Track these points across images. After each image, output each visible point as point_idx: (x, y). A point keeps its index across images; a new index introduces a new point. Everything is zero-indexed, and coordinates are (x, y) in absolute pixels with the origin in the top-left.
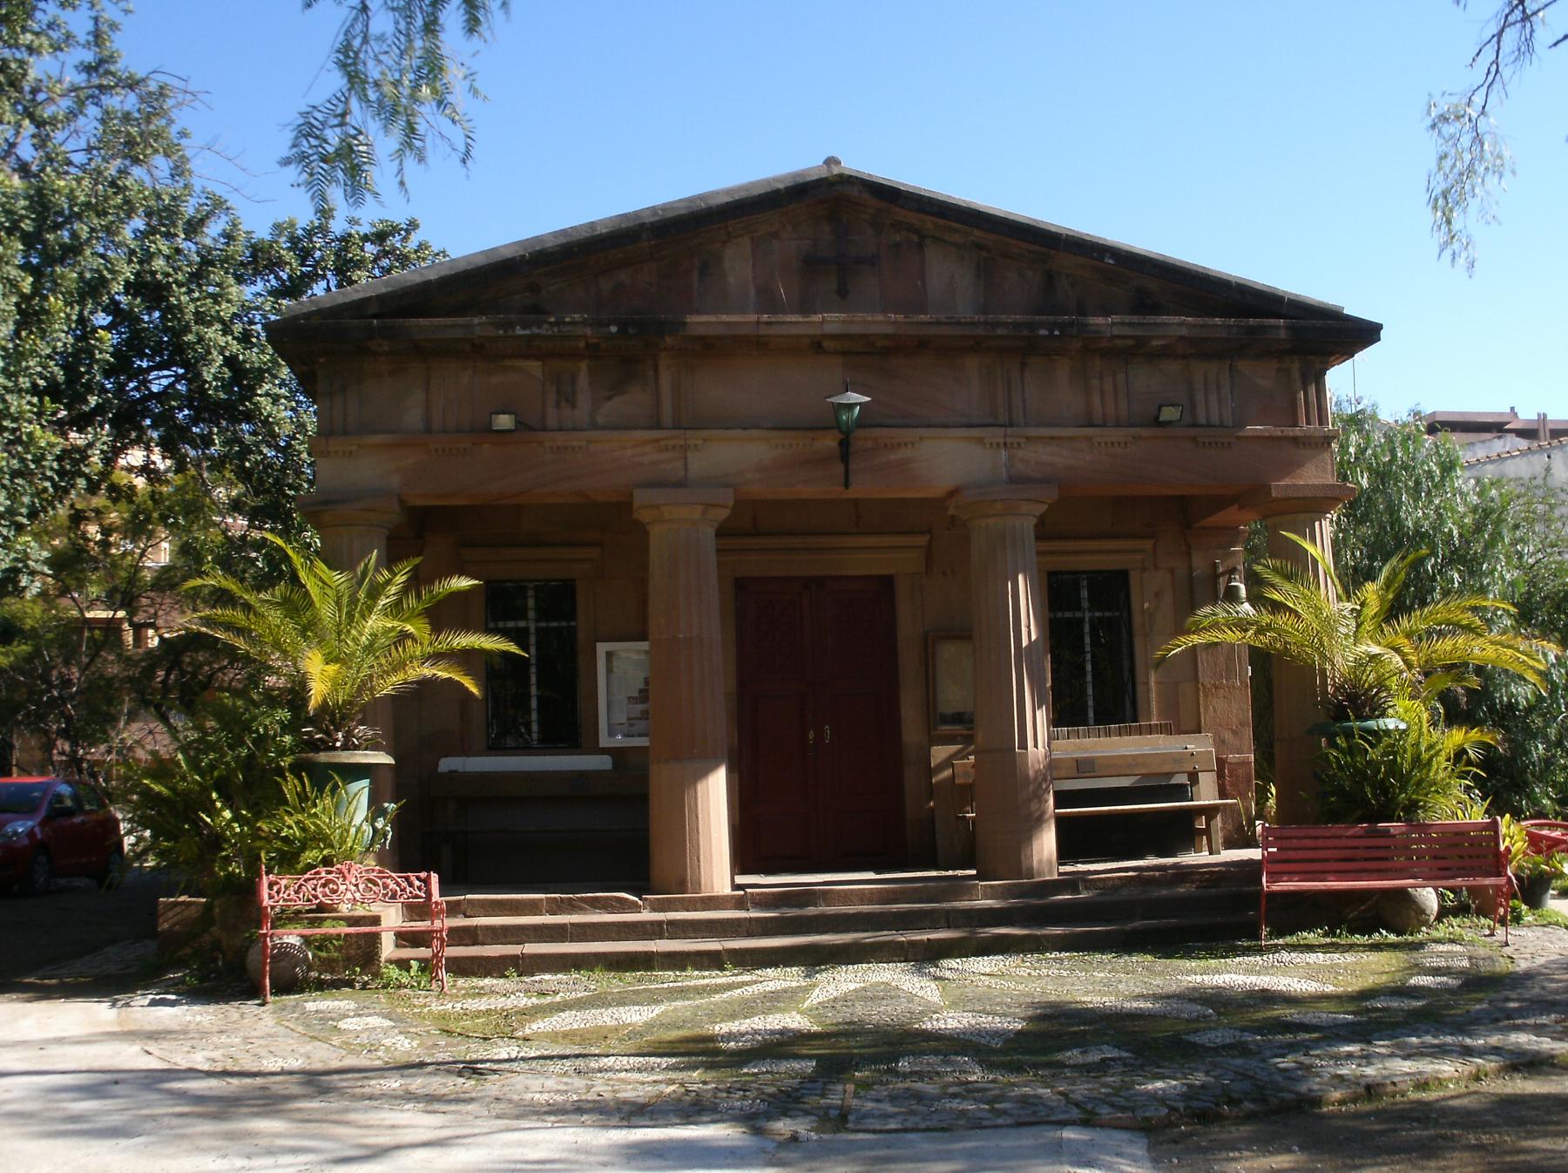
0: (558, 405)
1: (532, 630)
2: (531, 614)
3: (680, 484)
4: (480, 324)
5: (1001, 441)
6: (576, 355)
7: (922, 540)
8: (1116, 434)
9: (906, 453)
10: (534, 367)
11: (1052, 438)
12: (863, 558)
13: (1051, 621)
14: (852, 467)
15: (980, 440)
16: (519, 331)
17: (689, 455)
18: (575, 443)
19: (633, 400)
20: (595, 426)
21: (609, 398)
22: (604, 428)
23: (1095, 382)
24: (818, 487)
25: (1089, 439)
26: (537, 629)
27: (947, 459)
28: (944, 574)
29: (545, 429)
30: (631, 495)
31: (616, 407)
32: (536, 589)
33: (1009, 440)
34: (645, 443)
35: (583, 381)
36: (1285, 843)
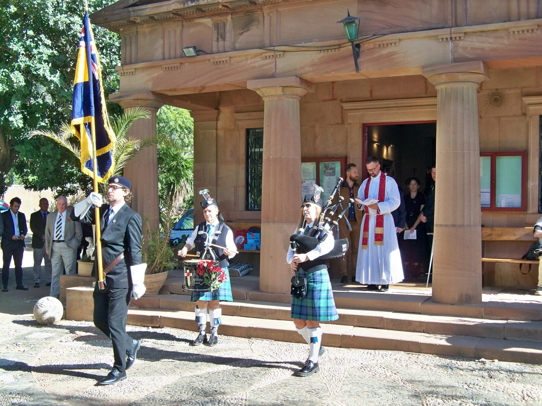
0: (218, 40)
3: (273, 76)
5: (449, 36)
6: (227, 14)
8: (525, 24)
9: (391, 49)
10: (208, 21)
11: (482, 32)
13: (258, 275)
15: (436, 37)
16: (190, 4)
17: (277, 60)
18: (223, 59)
19: (255, 33)
20: (235, 49)
24: (345, 73)
25: (507, 30)
27: (413, 52)
29: (212, 53)
30: (246, 83)
33: (453, 36)
34: (257, 55)
35: (229, 27)
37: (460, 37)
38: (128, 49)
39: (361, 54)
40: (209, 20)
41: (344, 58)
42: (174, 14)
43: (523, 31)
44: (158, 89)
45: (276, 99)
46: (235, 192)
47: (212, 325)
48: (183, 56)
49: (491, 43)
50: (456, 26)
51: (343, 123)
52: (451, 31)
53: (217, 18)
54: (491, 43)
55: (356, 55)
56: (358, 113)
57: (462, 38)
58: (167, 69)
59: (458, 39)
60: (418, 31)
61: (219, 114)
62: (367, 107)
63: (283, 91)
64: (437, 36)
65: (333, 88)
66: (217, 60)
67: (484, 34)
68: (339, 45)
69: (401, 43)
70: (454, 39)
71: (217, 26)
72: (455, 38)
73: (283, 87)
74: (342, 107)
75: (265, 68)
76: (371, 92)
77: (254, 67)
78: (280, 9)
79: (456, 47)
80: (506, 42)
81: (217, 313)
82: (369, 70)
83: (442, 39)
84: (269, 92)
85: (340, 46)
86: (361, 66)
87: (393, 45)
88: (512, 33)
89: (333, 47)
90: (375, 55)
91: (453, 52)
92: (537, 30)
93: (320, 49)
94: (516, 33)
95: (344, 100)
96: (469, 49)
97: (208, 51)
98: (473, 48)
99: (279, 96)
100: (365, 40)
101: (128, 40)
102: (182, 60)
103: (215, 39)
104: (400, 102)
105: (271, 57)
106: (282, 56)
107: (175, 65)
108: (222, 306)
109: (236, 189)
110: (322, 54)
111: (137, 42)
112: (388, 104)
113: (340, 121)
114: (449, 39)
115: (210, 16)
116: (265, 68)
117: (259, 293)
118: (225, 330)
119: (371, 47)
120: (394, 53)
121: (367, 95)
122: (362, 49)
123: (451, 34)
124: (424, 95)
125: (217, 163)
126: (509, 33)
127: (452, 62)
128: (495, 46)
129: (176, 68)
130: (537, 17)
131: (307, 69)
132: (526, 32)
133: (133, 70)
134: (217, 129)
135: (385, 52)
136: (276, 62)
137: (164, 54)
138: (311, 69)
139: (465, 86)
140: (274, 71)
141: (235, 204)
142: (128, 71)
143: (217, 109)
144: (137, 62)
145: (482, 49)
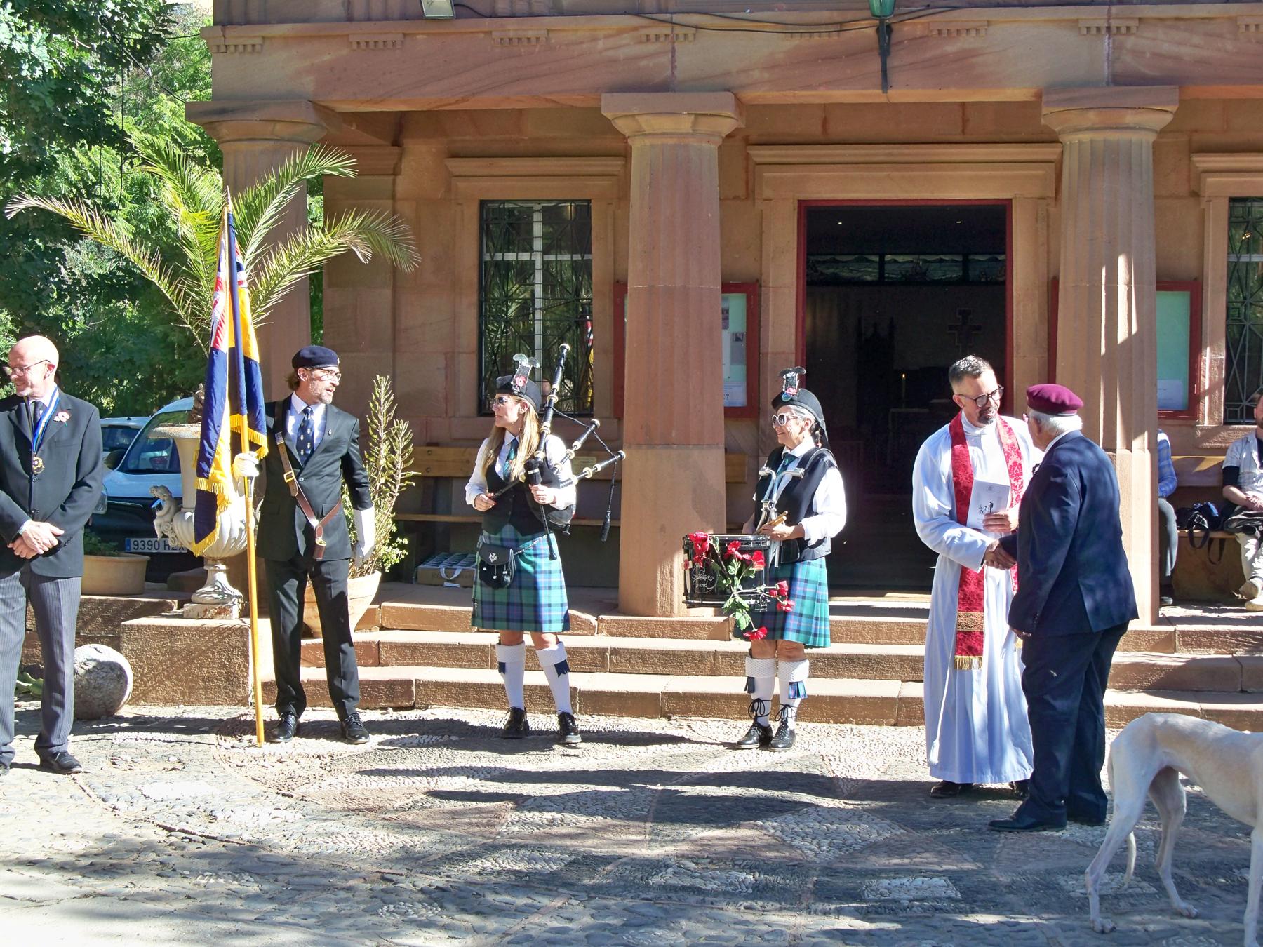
1: (538, 265)
2: (538, 245)
3: (664, 87)
11: (1177, 19)
12: (960, 181)
13: (616, 587)
14: (893, 62)
18: (530, 34)
24: (858, 92)
25: (1232, 20)
26: (544, 263)
29: (493, 15)
32: (545, 211)
33: (1114, 23)
34: (621, 32)
37: (1128, 28)
39: (893, 49)
41: (853, 55)
46: (447, 367)
47: (783, 701)
49: (1196, 46)
52: (1109, 12)
54: (1196, 46)
55: (885, 50)
56: (790, 174)
57: (1134, 30)
58: (363, 45)
59: (1124, 30)
60: (1033, 5)
62: (813, 160)
64: (1077, 21)
66: (511, 34)
68: (841, 23)
70: (1114, 31)
72: (1118, 28)
73: (696, 115)
74: (747, 157)
75: (643, 63)
77: (614, 61)
79: (1118, 48)
80: (1229, 46)
81: (801, 672)
83: (1088, 29)
84: (651, 129)
85: (841, 26)
86: (892, 77)
87: (973, 33)
88: (1243, 29)
89: (824, 29)
90: (928, 55)
91: (1112, 61)
93: (789, 29)
94: (1253, 28)
95: (754, 138)
96: (1148, 55)
98: (1155, 55)
100: (906, 17)
104: (880, 152)
105: (662, 39)
106: (691, 38)
107: (389, 38)
108: (811, 656)
109: (451, 358)
110: (796, 41)
112: (867, 155)
113: (741, 192)
114: (1104, 31)
116: (643, 63)
118: (820, 709)
119: (919, 33)
120: (972, 53)
121: (815, 130)
122: (895, 37)
123: (1109, 19)
124: (959, 138)
125: (395, 290)
126: (1238, 27)
127: (1108, 84)
129: (390, 45)
131: (756, 74)
133: (258, 41)
135: (951, 48)
136: (673, 51)
138: (766, 75)
139: (1134, 137)
140: (669, 73)
141: (446, 399)
142: (240, 41)
143: (396, 143)
144: (265, 21)
145: (1177, 58)
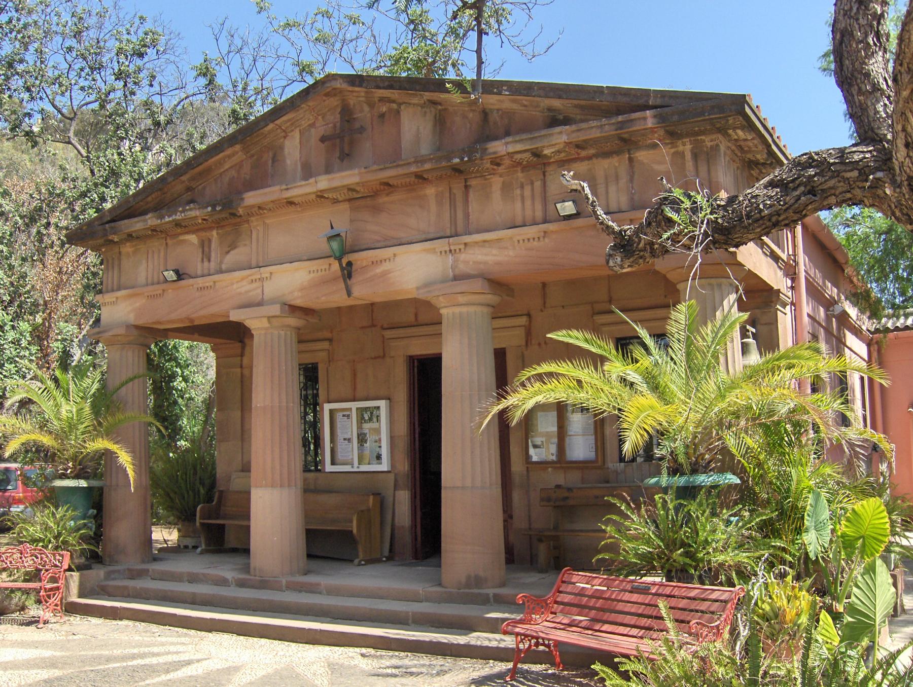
3: (260, 304)
4: (151, 220)
5: (448, 249)
6: (211, 228)
7: (523, 320)
8: (531, 231)
9: (386, 266)
10: (193, 238)
11: (485, 241)
15: (433, 251)
21: (228, 252)
22: (226, 272)
23: (518, 192)
24: (336, 297)
27: (410, 269)
28: (539, 344)
31: (232, 258)
33: (452, 248)
34: (243, 279)
36: (649, 611)
38: (110, 273)
40: (194, 236)
42: (153, 230)
43: (529, 240)
44: (140, 322)
45: (263, 332)
48: (166, 281)
50: (457, 235)
51: (384, 356)
53: (203, 234)
61: (243, 348)
63: (269, 322)
64: (435, 249)
65: (372, 311)
67: (487, 244)
69: (397, 259)
71: (202, 244)
73: (269, 318)
74: (383, 336)
75: (251, 294)
76: (416, 315)
77: (240, 294)
78: (267, 221)
79: (456, 261)
80: (511, 253)
82: (363, 292)
92: (544, 237)
94: (521, 242)
95: (385, 326)
97: (193, 275)
98: (474, 262)
99: (267, 329)
101: (110, 262)
102: (164, 286)
103: (200, 259)
111: (119, 265)
115: (193, 232)
116: (251, 294)
117: (248, 577)
121: (412, 319)
122: (354, 268)
128: (499, 259)
130: (545, 221)
131: (296, 294)
132: (531, 240)
134: (241, 367)
135: (379, 270)
137: (147, 278)
143: (242, 341)
144: (119, 289)
145: (485, 263)
